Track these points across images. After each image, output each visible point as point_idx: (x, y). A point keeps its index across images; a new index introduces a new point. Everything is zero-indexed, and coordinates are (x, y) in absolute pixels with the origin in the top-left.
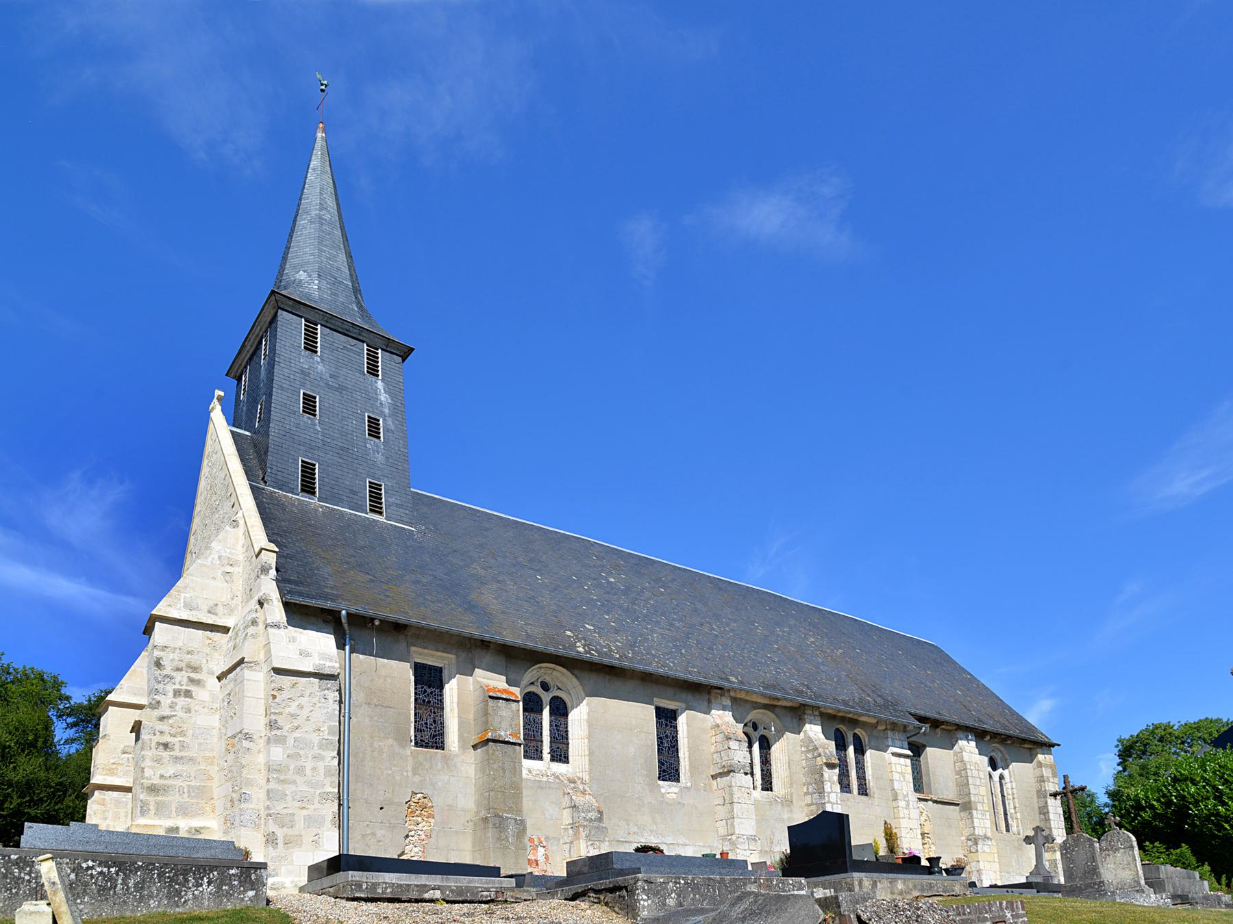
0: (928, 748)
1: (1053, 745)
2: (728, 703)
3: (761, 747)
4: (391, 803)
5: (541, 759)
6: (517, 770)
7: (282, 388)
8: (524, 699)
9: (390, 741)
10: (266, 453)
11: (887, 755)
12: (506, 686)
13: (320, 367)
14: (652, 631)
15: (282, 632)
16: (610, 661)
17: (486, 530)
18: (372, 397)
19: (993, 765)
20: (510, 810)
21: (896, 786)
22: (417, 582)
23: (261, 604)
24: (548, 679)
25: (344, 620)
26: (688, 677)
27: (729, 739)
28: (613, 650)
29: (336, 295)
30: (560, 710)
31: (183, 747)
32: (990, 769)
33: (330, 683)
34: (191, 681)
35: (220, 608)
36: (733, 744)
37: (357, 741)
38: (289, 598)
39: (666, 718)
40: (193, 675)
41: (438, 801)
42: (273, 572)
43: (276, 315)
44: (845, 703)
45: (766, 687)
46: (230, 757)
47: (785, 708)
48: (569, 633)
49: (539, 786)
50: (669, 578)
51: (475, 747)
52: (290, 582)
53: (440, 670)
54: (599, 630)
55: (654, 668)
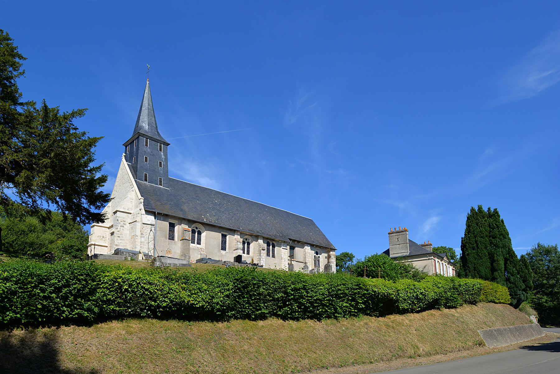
0: (296, 248)
1: (336, 250)
2: (239, 234)
3: (247, 244)
4: (163, 250)
5: (195, 244)
6: (189, 245)
7: (140, 156)
8: (192, 231)
9: (164, 238)
10: (137, 171)
11: (281, 248)
12: (188, 228)
13: (149, 150)
14: (224, 216)
15: (144, 216)
16: (211, 223)
17: (186, 188)
18: (160, 157)
19: (317, 253)
20: (187, 254)
21: (282, 256)
22: (170, 204)
23: (140, 210)
24: (197, 226)
25: (156, 214)
26: (230, 228)
27: (238, 242)
28: (212, 220)
29: (152, 130)
30: (200, 233)
31: (122, 237)
32: (315, 254)
33: (153, 226)
34: (124, 224)
35: (129, 209)
36: (239, 243)
37: (157, 238)
38: (146, 209)
39: (224, 236)
40: (124, 223)
41: (173, 251)
42: (143, 203)
43: (139, 137)
44: (270, 235)
45: (249, 231)
46: (133, 240)
47: (254, 235)
48: (203, 216)
49: (194, 249)
50: (232, 200)
51: (181, 240)
52: (146, 205)
53: (174, 224)
54: (210, 216)
55: (222, 225)
